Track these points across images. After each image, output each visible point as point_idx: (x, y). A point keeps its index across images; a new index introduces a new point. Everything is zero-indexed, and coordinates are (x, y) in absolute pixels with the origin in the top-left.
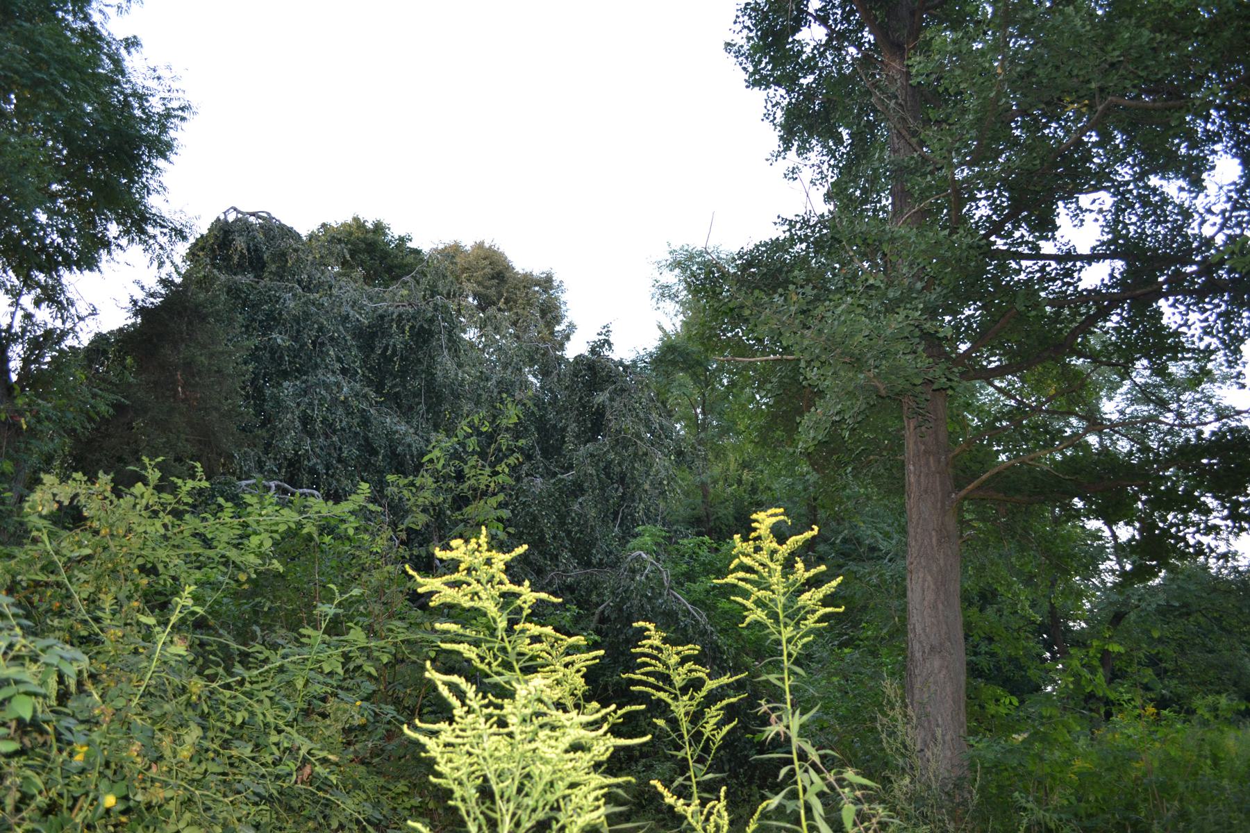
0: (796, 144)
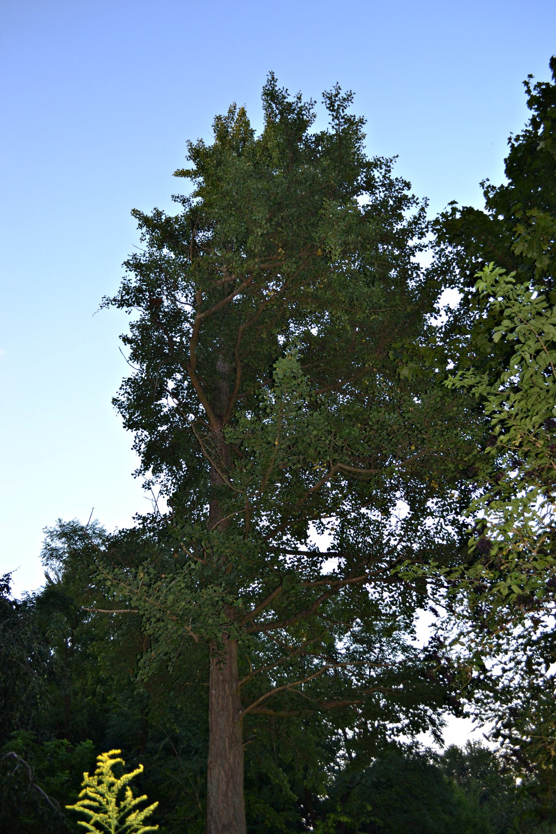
0: (152, 466)
